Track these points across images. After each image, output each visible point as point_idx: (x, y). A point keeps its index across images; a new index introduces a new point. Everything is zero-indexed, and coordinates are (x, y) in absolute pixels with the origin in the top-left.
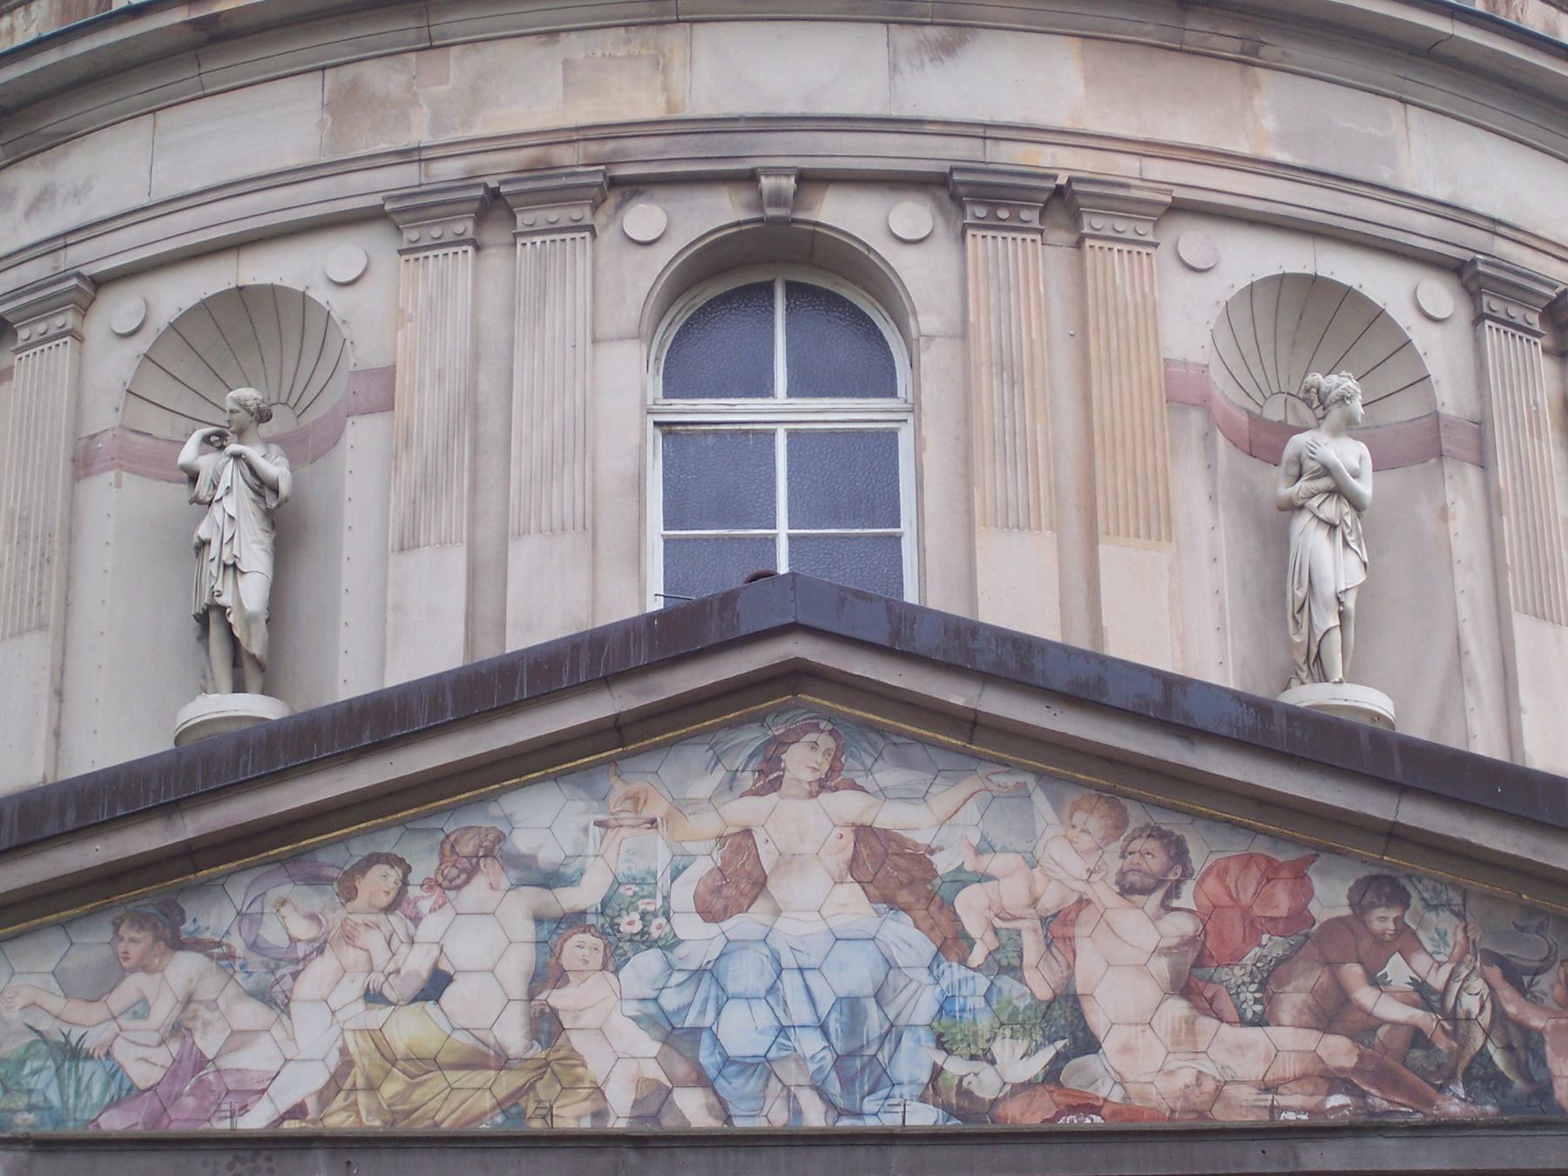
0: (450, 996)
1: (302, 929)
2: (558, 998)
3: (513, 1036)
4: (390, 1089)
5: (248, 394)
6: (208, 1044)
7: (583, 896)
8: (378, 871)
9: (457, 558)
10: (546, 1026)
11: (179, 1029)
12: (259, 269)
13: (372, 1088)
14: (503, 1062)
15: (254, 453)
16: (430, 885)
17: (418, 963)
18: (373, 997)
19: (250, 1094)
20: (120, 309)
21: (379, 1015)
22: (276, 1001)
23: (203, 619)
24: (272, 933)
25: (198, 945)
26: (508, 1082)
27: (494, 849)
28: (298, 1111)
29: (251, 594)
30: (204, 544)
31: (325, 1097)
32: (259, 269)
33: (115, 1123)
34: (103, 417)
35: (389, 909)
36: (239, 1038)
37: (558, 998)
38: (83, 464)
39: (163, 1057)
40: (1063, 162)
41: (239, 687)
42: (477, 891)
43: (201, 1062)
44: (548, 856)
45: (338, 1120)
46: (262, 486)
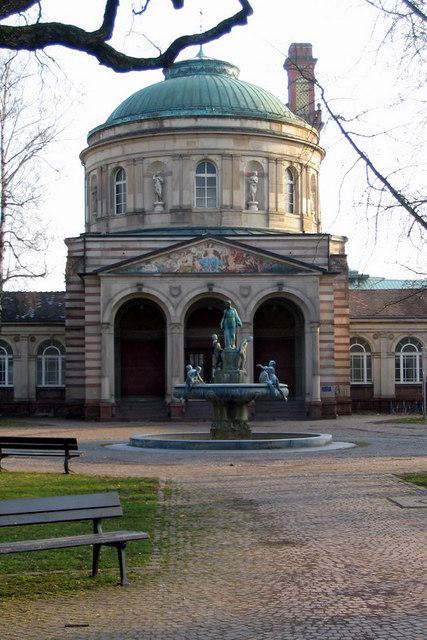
12: (160, 159)
20: (146, 161)
27: (190, 252)
32: (160, 159)
40: (231, 152)
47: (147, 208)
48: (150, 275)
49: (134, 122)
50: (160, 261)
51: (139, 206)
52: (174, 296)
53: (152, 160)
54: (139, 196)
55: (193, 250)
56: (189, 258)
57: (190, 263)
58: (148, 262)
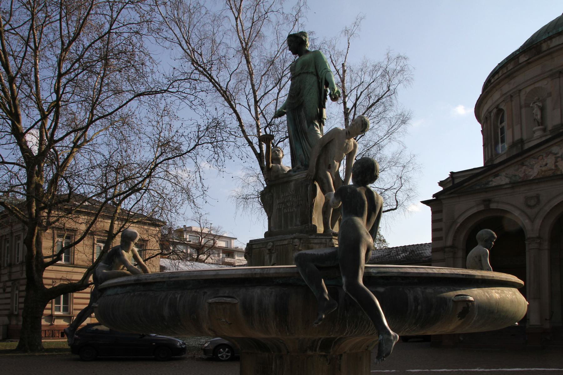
0: (548, 165)
1: (534, 162)
2: (557, 164)
3: (553, 167)
4: (543, 173)
5: (537, 98)
6: (527, 173)
7: (559, 155)
8: (540, 157)
9: (559, 110)
10: (556, 166)
11: (524, 172)
12: (537, 85)
13: (541, 174)
14: (552, 170)
15: (538, 103)
16: (545, 157)
17: (544, 163)
18: (541, 167)
19: (530, 176)
20: (523, 93)
21: (541, 168)
22: (532, 168)
23: (535, 120)
24: (532, 163)
25: (525, 165)
26: (553, 171)
27: (551, 153)
28: (535, 177)
29: (539, 117)
30: (534, 113)
31: (537, 175)
33: (520, 180)
34: (523, 103)
35: (542, 159)
36: (530, 172)
37: (557, 164)
38: (521, 108)
39: (523, 174)
41: (539, 126)
42: (549, 156)
43: (526, 174)
44: (556, 152)
45: (538, 177)
46: (539, 106)
47: (525, 137)
48: (499, 188)
49: (544, 79)
50: (511, 171)
51: (517, 137)
52: (529, 207)
53: (528, 90)
54: (517, 128)
55: (555, 149)
56: (550, 161)
57: (551, 165)
58: (496, 175)
